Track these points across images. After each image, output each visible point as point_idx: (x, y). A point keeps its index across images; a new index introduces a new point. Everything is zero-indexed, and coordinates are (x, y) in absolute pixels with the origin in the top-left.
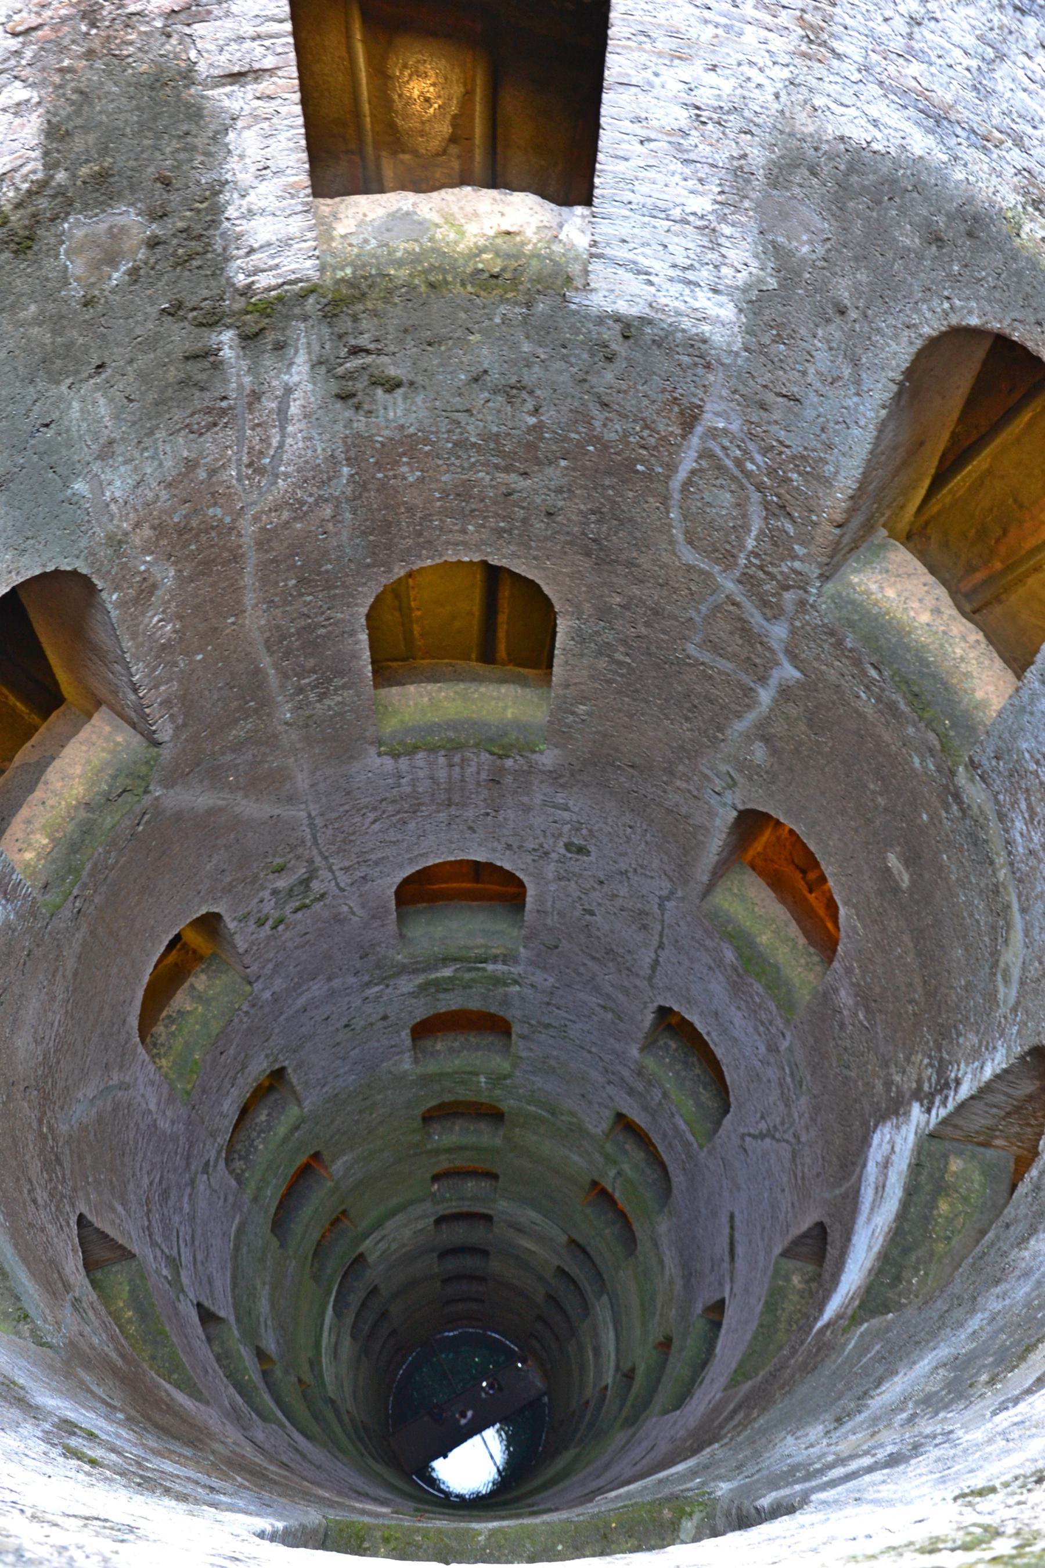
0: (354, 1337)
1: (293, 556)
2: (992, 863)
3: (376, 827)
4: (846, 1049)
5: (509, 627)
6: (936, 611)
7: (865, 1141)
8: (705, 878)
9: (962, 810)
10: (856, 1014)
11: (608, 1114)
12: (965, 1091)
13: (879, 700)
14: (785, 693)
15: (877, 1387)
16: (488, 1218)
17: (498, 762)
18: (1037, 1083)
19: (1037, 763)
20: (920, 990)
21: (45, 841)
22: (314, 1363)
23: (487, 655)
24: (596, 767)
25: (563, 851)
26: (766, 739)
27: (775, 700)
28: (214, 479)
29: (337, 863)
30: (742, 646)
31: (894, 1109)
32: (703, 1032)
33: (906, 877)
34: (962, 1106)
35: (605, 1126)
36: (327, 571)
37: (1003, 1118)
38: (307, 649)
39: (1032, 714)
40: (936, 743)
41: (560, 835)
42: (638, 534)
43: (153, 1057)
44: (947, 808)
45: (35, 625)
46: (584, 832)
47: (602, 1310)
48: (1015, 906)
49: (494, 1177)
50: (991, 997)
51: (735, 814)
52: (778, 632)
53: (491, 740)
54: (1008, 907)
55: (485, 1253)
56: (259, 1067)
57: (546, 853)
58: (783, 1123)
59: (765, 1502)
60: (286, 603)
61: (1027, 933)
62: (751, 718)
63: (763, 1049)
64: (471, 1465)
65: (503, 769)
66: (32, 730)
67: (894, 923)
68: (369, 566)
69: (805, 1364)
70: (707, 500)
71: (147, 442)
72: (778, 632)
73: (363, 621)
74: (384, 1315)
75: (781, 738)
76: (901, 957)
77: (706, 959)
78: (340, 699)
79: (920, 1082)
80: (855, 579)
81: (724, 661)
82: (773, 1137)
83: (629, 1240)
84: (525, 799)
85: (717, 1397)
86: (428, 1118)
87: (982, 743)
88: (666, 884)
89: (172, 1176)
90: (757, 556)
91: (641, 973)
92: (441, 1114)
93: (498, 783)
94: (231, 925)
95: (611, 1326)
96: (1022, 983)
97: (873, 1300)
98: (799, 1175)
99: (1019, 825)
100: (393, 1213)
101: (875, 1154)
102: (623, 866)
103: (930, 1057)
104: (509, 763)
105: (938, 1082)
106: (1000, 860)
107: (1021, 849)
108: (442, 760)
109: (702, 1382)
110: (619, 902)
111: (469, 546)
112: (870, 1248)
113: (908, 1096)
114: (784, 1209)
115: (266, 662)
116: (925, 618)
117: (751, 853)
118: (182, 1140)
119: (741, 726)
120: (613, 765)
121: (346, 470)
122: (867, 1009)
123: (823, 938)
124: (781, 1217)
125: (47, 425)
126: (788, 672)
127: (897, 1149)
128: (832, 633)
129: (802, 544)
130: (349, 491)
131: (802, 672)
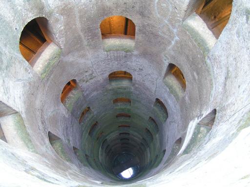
5: (128, 29)
7: (188, 124)
11: (148, 117)
12: (204, 116)
14: (177, 42)
22: (98, 157)
23: (126, 33)
24: (145, 54)
27: (175, 43)
31: (193, 119)
34: (203, 119)
35: (148, 119)
38: (89, 31)
47: (148, 150)
53: (124, 49)
61: (215, 88)
64: (128, 173)
65: (127, 54)
66: (41, 45)
72: (175, 31)
86: (117, 116)
97: (186, 152)
100: (112, 132)
101: (190, 126)
109: (160, 162)
115: (81, 34)
118: (70, 119)
122: (190, 101)
123: (184, 86)
126: (177, 38)
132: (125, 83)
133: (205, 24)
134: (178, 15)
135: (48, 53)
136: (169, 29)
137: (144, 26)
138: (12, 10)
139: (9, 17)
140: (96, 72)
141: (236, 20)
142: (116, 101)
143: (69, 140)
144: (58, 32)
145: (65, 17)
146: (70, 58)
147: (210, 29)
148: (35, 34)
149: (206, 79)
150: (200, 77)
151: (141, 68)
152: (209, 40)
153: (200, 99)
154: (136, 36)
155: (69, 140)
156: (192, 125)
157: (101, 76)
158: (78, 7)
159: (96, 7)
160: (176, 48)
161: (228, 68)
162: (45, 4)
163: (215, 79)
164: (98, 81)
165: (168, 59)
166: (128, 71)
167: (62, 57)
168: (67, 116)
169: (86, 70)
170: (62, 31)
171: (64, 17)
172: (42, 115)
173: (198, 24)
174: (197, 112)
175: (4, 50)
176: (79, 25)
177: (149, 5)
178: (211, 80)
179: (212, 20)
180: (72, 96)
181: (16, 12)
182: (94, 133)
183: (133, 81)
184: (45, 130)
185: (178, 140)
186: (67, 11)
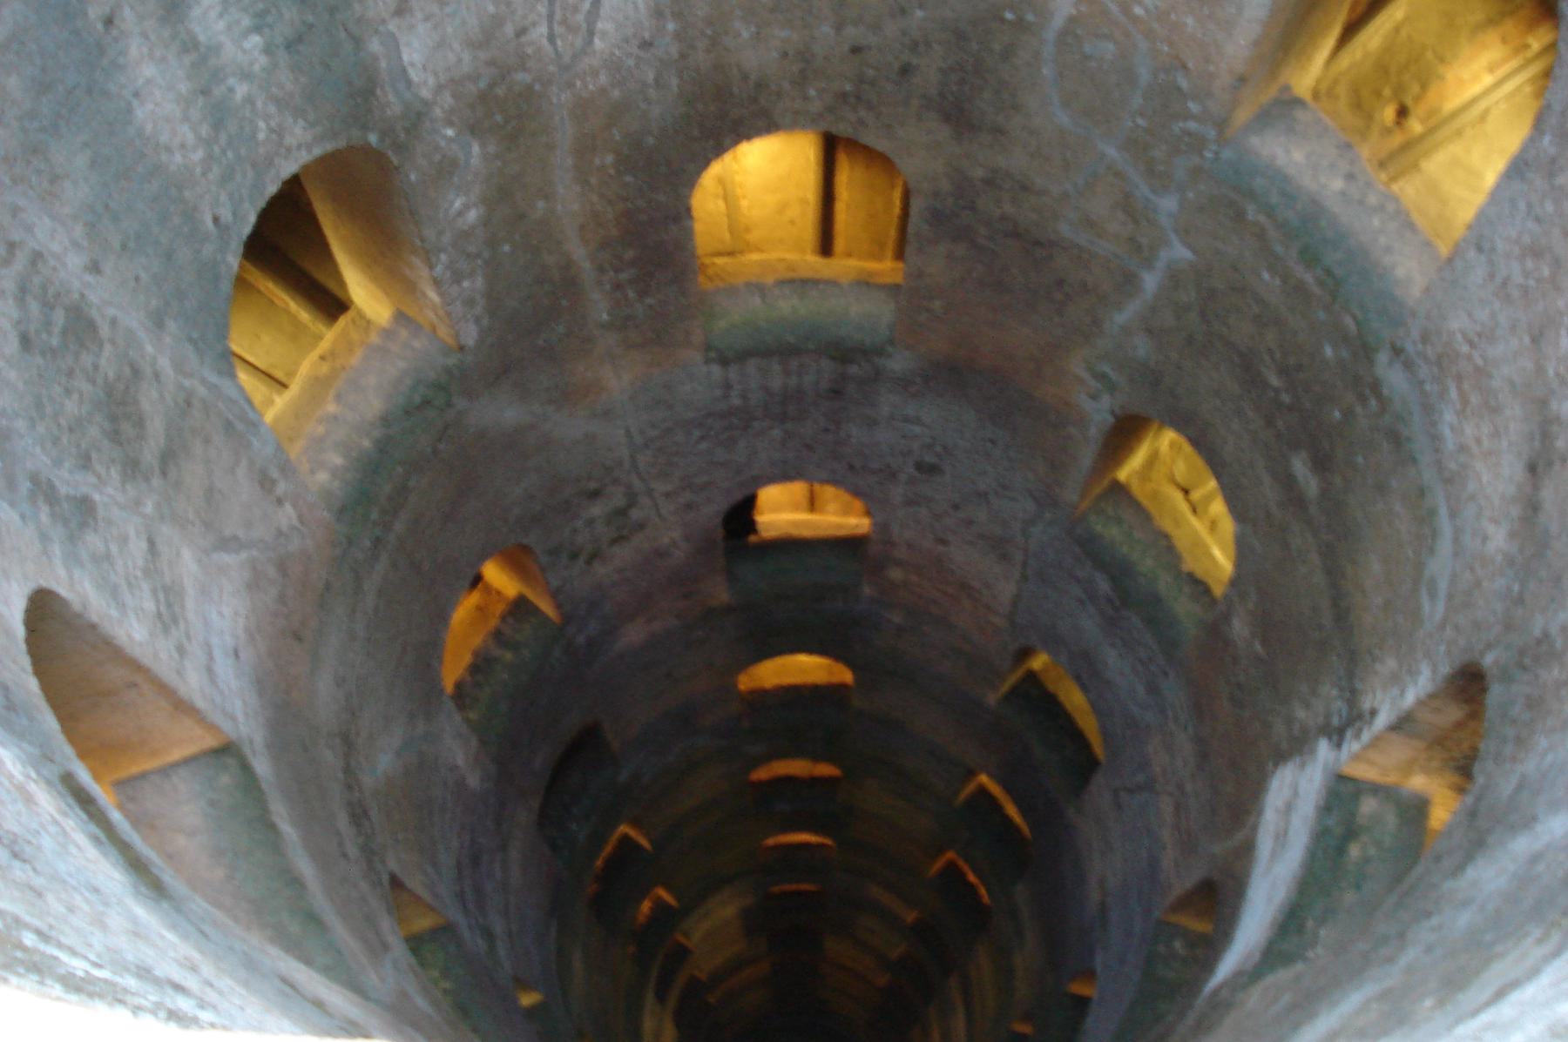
13: (1285, 281)
14: (1174, 278)
19: (1472, 344)
25: (912, 470)
26: (1149, 331)
28: (523, 39)
29: (660, 487)
31: (1297, 746)
46: (938, 449)
48: (1443, 512)
51: (1111, 420)
52: (1168, 204)
54: (1432, 512)
61: (1456, 540)
63: (1141, 690)
79: (1328, 716)
96: (1450, 597)
97: (1274, 954)
99: (1449, 417)
104: (853, 370)
108: (777, 368)
116: (1338, 184)
122: (1265, 642)
130: (674, 50)
134: (1193, 107)
138: (201, 101)
139: (183, 146)
140: (650, 492)
143: (489, 935)
144: (446, 238)
145: (491, 149)
146: (502, 412)
150: (1338, 480)
151: (929, 459)
152: (1388, 250)
155: (489, 935)
158: (571, 85)
159: (674, 82)
161: (1543, 403)
162: (383, 64)
163: (1449, 481)
164: (661, 553)
165: (1112, 388)
167: (461, 403)
169: (593, 485)
170: (466, 235)
171: (483, 145)
172: (347, 770)
174: (1329, 697)
175: (149, 349)
177: (1007, 54)
178: (1422, 492)
181: (219, 114)
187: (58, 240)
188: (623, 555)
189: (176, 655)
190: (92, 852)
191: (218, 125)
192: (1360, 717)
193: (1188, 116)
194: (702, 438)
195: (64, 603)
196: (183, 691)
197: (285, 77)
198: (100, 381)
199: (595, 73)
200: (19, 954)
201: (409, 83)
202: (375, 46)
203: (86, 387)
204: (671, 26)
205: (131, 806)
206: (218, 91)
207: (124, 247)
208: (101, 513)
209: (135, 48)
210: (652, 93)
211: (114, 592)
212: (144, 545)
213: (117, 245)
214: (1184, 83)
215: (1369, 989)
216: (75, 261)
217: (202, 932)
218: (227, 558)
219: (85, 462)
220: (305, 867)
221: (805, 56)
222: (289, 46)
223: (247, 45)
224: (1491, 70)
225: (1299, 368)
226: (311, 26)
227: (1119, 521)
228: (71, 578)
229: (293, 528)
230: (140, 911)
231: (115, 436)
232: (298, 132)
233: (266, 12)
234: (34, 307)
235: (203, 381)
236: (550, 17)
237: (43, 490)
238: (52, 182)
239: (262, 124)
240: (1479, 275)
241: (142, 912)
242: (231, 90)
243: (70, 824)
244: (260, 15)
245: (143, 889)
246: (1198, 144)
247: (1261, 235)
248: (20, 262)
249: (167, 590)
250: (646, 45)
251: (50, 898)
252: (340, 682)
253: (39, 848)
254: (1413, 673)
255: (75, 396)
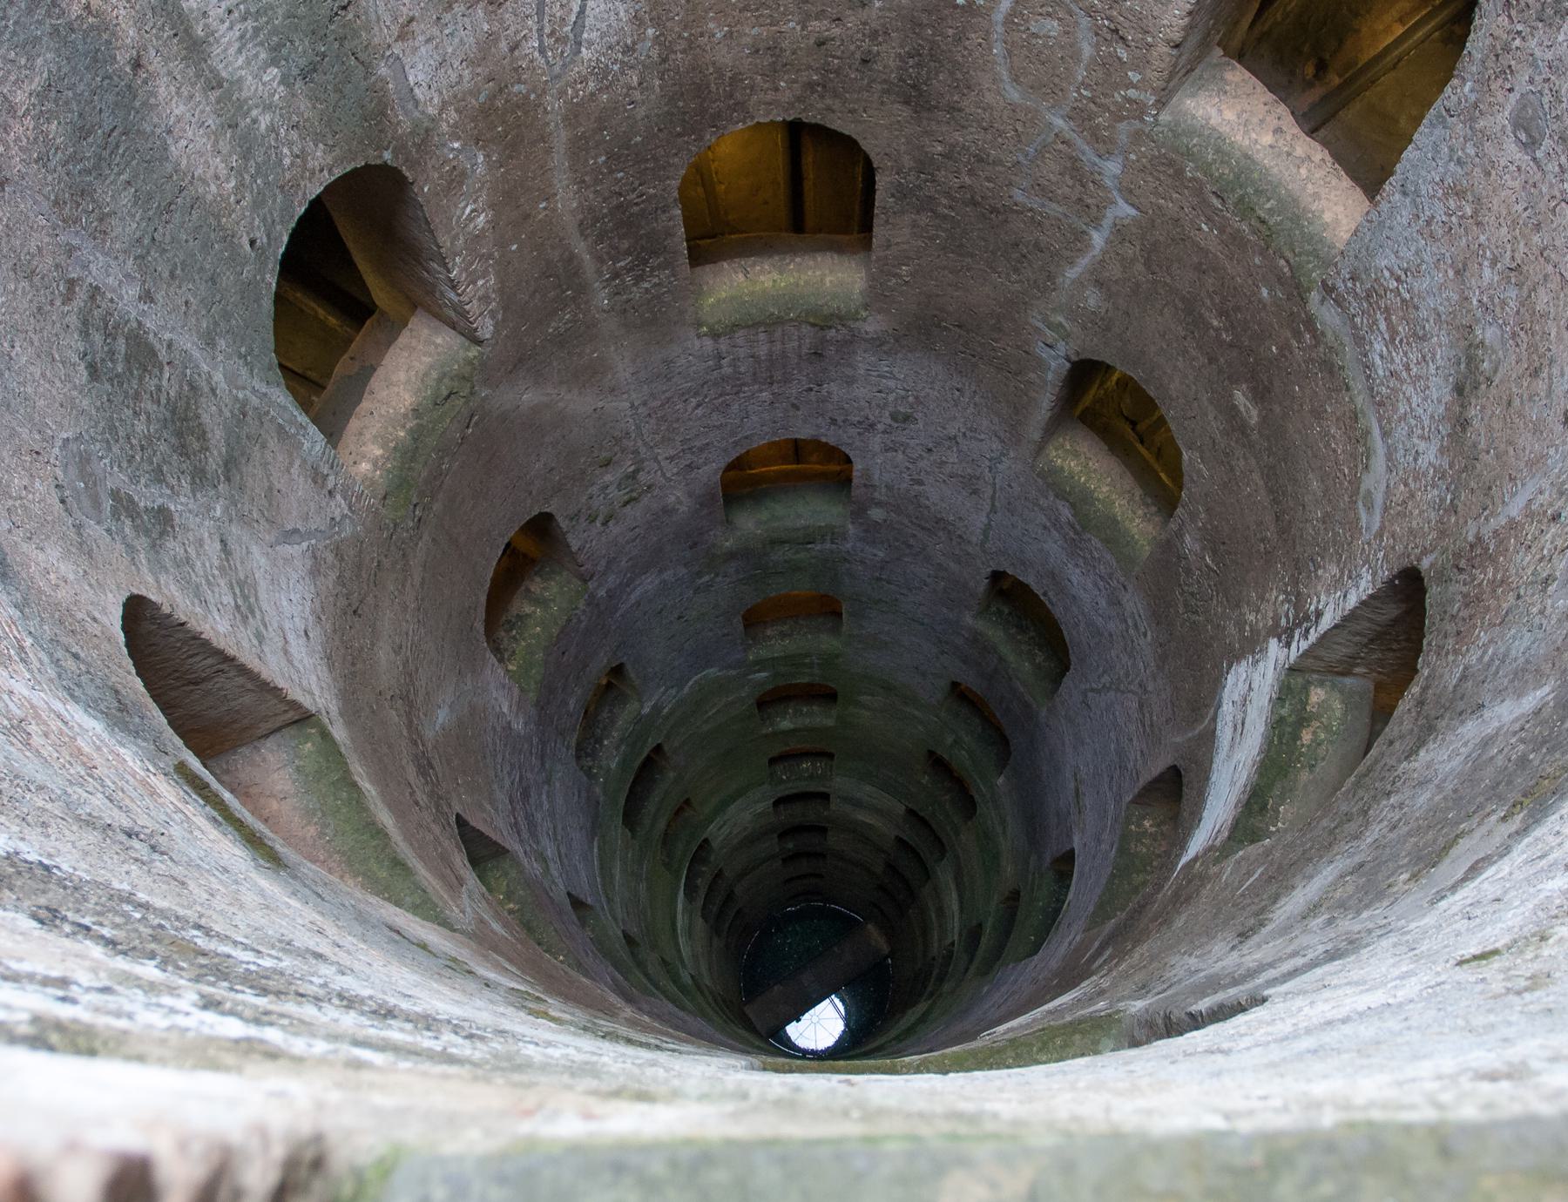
0: (703, 916)
1: (601, 130)
2: (1348, 389)
3: (699, 412)
4: (1192, 594)
5: (818, 184)
6: (1278, 131)
8: (1037, 436)
9: (1314, 337)
10: (1203, 558)
12: (1327, 622)
13: (1222, 231)
15: (1275, 902)
16: (825, 797)
17: (820, 334)
18: (1404, 606)
19: (1398, 279)
20: (1272, 528)
21: (379, 452)
24: (926, 329)
25: (889, 421)
26: (1099, 283)
29: (663, 452)
30: (1072, 187)
31: (1251, 646)
32: (1039, 593)
33: (1254, 413)
36: (636, 144)
37: (1365, 646)
38: (622, 228)
39: (1391, 228)
40: (1286, 270)
41: (886, 405)
42: (959, 76)
43: (501, 660)
44: (1298, 335)
45: (340, 229)
47: (944, 875)
48: (1376, 432)
49: (831, 756)
50: (1354, 526)
51: (1068, 365)
52: (1112, 167)
54: (1367, 433)
55: (823, 830)
56: (601, 662)
57: (872, 426)
58: (1127, 675)
59: (1203, 1005)
60: (597, 181)
61: (1389, 457)
62: (1084, 262)
63: (1103, 603)
64: (821, 1025)
67: (1242, 463)
68: (679, 135)
69: (1176, 895)
70: (1033, 30)
71: (447, 17)
73: (676, 194)
74: (730, 897)
75: (1116, 282)
76: (1250, 495)
77: (1042, 519)
78: (656, 280)
80: (1189, 103)
81: (1054, 205)
82: (1118, 690)
83: (968, 805)
84: (849, 371)
85: (1078, 938)
87: (1336, 265)
88: (996, 445)
89: (529, 775)
90: (1087, 87)
91: (974, 539)
92: (769, 701)
93: (821, 355)
94: (564, 524)
95: (953, 886)
96: (1386, 509)
98: (1147, 723)
99: (1379, 346)
100: (733, 799)
102: (953, 432)
103: (1285, 592)
105: (1296, 616)
106: (1358, 385)
107: (1381, 372)
110: (948, 469)
111: (777, 102)
112: (1233, 783)
113: (1263, 633)
114: (1132, 757)
115: (580, 247)
116: (1268, 139)
117: (1080, 408)
118: (535, 740)
119: (1072, 273)
120: (938, 326)
121: (650, 32)
122: (1214, 552)
124: (1130, 765)
125: (344, 8)
126: (1123, 210)
127: (1255, 686)
128: (1171, 163)
129: (1136, 69)
130: (655, 53)
131: (1138, 209)
132: (809, 511)
133: (1282, 109)
134: (1134, 76)
135: (407, 373)
136: (1074, 160)
137: (924, 165)
139: (217, 178)
141: (1507, 49)
142: (754, 620)
143: (542, 858)
147: (1312, 132)
148: (340, 267)
149: (1318, 414)
150: (1277, 409)
152: (1316, 196)
153: (1283, 531)
154: (879, 232)
155: (542, 858)
156: (1250, 691)
157: (678, 483)
158: (562, 93)
160: (1115, 271)
165: (1066, 337)
166: (830, 437)
168: (518, 725)
171: (487, 156)
172: (410, 725)
173: (1241, 118)
174: (1277, 603)
176: (565, 199)
179: (1309, 85)
180: (528, 609)
181: (246, 144)
182: (651, 806)
183: (857, 491)
184: (437, 806)
185: (1159, 779)
186: (503, 118)
187: (111, 274)
188: (634, 513)
189: (255, 642)
190: (214, 833)
191: (246, 156)
192: (1307, 618)
193: (1131, 85)
194: (698, 406)
195: (155, 607)
196: (265, 675)
197: (304, 104)
198: (163, 401)
199: (584, 80)
200: (203, 961)
201: (417, 103)
202: (383, 70)
203: (150, 406)
204: (650, 32)
205: (225, 778)
206: (244, 123)
207: (172, 275)
208: (177, 521)
209: (163, 89)
210: (637, 95)
211: (197, 593)
212: (218, 546)
213: (166, 275)
214: (1123, 54)
215: (1342, 864)
216: (132, 291)
217: (319, 896)
218: (288, 550)
219: (159, 477)
220: (386, 818)
221: (774, 49)
222: (304, 75)
223: (266, 78)
224: (1401, 20)
225: (1237, 309)
226: (324, 56)
227: (1076, 455)
228: (158, 582)
229: (344, 516)
230: (264, 882)
231: (183, 450)
232: (319, 156)
233: (281, 45)
234: (98, 338)
235: (254, 391)
236: (540, 30)
237: (124, 505)
238: (101, 220)
239: (285, 150)
240: (1404, 216)
241: (266, 883)
242: (255, 121)
243: (189, 809)
244: (275, 49)
245: (262, 862)
246: (1139, 110)
247: (1199, 192)
248: (81, 294)
249: (241, 584)
250: (628, 50)
251: (192, 885)
252: (398, 650)
253: (171, 838)
254: (1355, 578)
255: (143, 417)
